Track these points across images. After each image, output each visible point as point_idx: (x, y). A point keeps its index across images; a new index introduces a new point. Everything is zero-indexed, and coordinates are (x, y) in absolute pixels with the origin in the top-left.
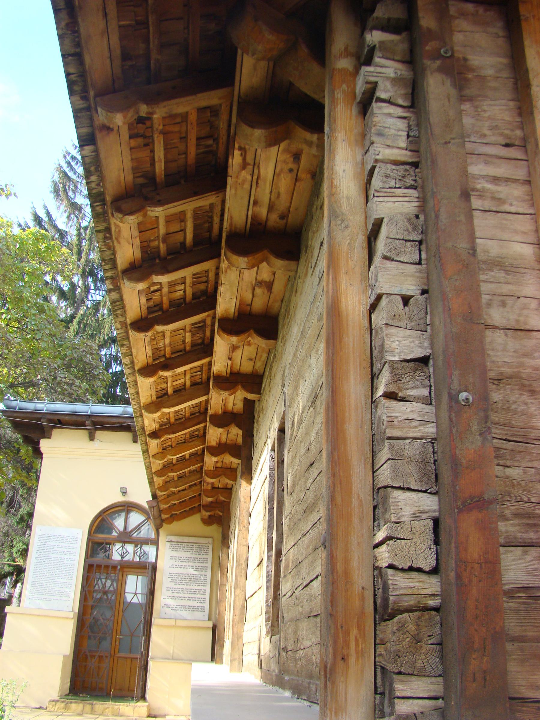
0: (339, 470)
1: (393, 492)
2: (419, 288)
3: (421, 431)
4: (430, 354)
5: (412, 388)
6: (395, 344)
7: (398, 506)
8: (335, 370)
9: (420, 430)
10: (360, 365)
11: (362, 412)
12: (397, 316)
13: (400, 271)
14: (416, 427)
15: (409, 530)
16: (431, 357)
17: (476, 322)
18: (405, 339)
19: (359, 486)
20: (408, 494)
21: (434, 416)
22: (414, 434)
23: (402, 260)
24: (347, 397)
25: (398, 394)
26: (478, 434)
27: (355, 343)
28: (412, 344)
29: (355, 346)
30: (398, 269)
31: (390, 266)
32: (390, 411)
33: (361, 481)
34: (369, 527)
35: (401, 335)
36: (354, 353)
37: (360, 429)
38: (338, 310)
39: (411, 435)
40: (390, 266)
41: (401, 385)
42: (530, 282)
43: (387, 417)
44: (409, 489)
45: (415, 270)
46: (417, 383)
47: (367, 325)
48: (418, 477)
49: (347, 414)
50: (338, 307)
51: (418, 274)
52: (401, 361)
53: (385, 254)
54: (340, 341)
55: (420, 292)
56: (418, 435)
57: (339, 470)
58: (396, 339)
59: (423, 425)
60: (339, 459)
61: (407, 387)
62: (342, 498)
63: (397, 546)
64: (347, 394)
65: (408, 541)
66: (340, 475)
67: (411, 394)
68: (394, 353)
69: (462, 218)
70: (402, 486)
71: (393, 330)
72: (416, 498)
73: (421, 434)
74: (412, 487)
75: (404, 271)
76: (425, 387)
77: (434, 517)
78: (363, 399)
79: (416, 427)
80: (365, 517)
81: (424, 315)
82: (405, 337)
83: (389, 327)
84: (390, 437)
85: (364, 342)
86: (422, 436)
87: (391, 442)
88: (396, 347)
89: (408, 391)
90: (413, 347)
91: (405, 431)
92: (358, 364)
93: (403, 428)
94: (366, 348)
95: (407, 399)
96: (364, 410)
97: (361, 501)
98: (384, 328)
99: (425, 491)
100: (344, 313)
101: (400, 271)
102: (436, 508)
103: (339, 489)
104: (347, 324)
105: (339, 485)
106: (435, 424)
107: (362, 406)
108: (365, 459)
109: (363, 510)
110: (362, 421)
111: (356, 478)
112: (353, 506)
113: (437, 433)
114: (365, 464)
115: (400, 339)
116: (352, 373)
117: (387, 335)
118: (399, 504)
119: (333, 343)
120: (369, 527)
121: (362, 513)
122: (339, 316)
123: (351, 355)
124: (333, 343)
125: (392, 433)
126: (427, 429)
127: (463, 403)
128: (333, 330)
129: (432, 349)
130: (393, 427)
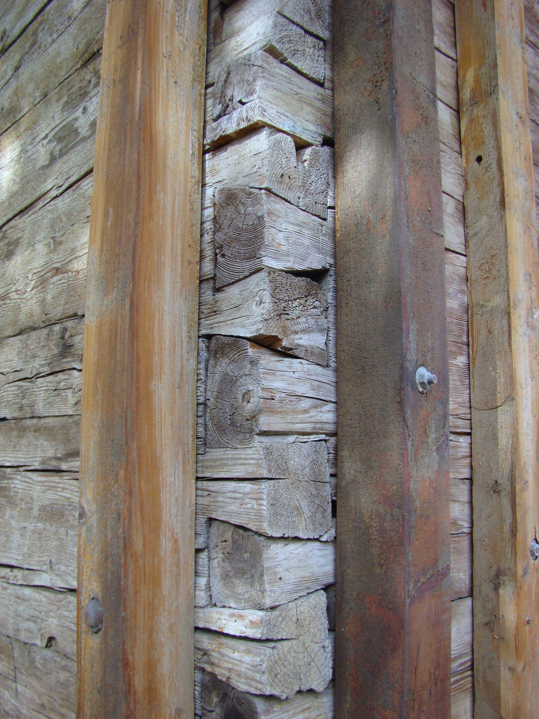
0: (139, 480)
1: (268, 547)
2: (320, 131)
3: (313, 420)
4: (331, 265)
5: (304, 331)
6: (281, 235)
7: (275, 573)
8: (138, 258)
9: (311, 417)
10: (182, 257)
11: (182, 356)
12: (286, 178)
13: (293, 87)
14: (306, 411)
15: (294, 619)
16: (331, 272)
17: (436, 231)
18: (297, 228)
19: (174, 511)
20: (292, 547)
21: (333, 389)
22: (303, 425)
23: (299, 65)
24: (156, 322)
25: (281, 340)
26: (434, 448)
27: (176, 208)
28: (307, 242)
29: (176, 213)
30: (290, 82)
31: (278, 71)
32: (268, 377)
33: (177, 500)
34: (189, 591)
35: (292, 220)
36: (173, 227)
37: (177, 390)
38: (151, 129)
39: (298, 427)
40: (278, 71)
41: (288, 323)
42: (449, 168)
43: (263, 389)
44: (297, 539)
45: (315, 94)
46: (312, 321)
47: (197, 173)
48: (309, 514)
49: (156, 358)
50: (151, 123)
51: (318, 104)
52: (287, 272)
53: (274, 43)
54: (151, 199)
55: (320, 139)
56: (308, 427)
57: (139, 480)
58: (284, 226)
59: (316, 407)
60: (139, 456)
61: (297, 328)
62: (144, 539)
63: (277, 657)
64: (157, 316)
65: (294, 642)
66: (141, 490)
67: (301, 342)
68: (277, 255)
69: (421, 26)
70: (286, 536)
71: (279, 206)
72: (302, 553)
73: (312, 425)
74: (301, 536)
75: (299, 91)
76: (321, 331)
77: (324, 585)
78: (185, 328)
79: (306, 411)
80: (182, 572)
81: (324, 187)
82: (298, 225)
83: (273, 198)
84: (265, 432)
85: (192, 209)
86: (314, 428)
87: (265, 439)
88: (283, 242)
89: (297, 336)
90: (308, 247)
91: (289, 418)
92: (179, 252)
93: (286, 413)
94: (194, 222)
95: (296, 352)
96: (185, 351)
97: (176, 541)
98: (264, 196)
99: (317, 540)
100: (161, 140)
101: (293, 87)
102: (329, 568)
103: (139, 521)
104: (165, 164)
105: (139, 514)
106: (333, 405)
107: (182, 342)
108: (184, 455)
109: (179, 560)
110: (182, 374)
111: (168, 497)
112: (162, 553)
113: (336, 423)
114: (184, 465)
115: (290, 227)
116: (168, 270)
117: (270, 213)
118: (279, 569)
119: (138, 199)
120: (189, 591)
121: (178, 566)
122: (151, 143)
123: (169, 232)
124: (138, 199)
125: (269, 424)
126: (321, 414)
127: (421, 389)
128: (138, 171)
129: (335, 256)
130: (272, 411)
